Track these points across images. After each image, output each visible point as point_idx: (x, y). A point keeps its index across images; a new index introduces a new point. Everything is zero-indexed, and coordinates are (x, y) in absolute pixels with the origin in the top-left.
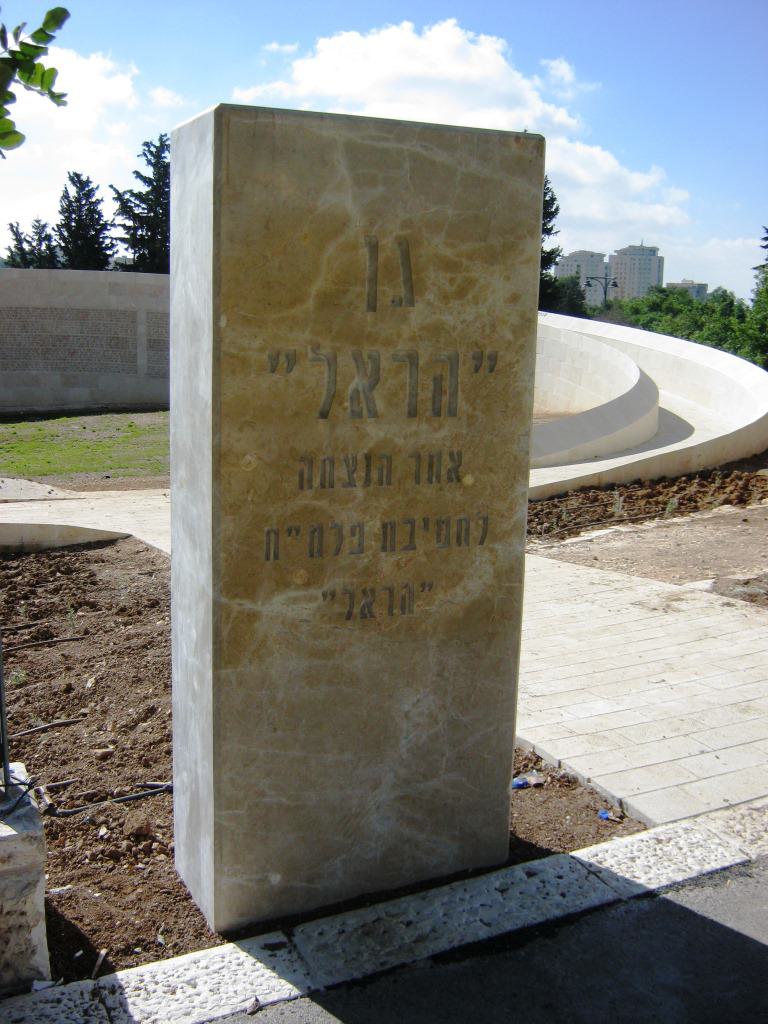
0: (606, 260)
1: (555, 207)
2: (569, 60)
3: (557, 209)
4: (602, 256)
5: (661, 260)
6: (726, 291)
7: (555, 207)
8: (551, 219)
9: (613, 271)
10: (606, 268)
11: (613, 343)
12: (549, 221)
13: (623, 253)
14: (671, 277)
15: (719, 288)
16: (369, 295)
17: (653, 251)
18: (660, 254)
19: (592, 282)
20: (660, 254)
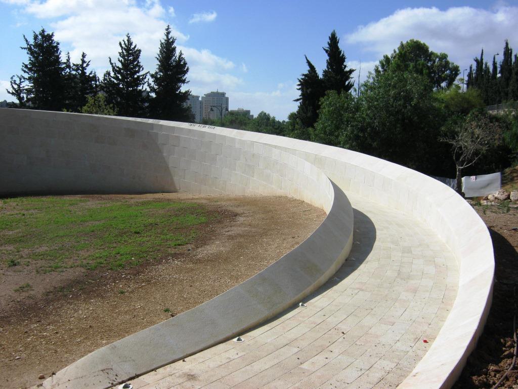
0: (200, 99)
1: (186, 68)
2: (174, 8)
3: (188, 69)
4: (198, 97)
5: (227, 99)
6: (266, 113)
7: (186, 68)
8: (185, 74)
9: (204, 105)
10: (200, 103)
11: (286, 149)
12: (184, 76)
13: (208, 95)
14: (232, 107)
15: (262, 112)
16: (193, 199)
17: (223, 94)
18: (226, 96)
19: (213, 108)
20: (226, 96)
